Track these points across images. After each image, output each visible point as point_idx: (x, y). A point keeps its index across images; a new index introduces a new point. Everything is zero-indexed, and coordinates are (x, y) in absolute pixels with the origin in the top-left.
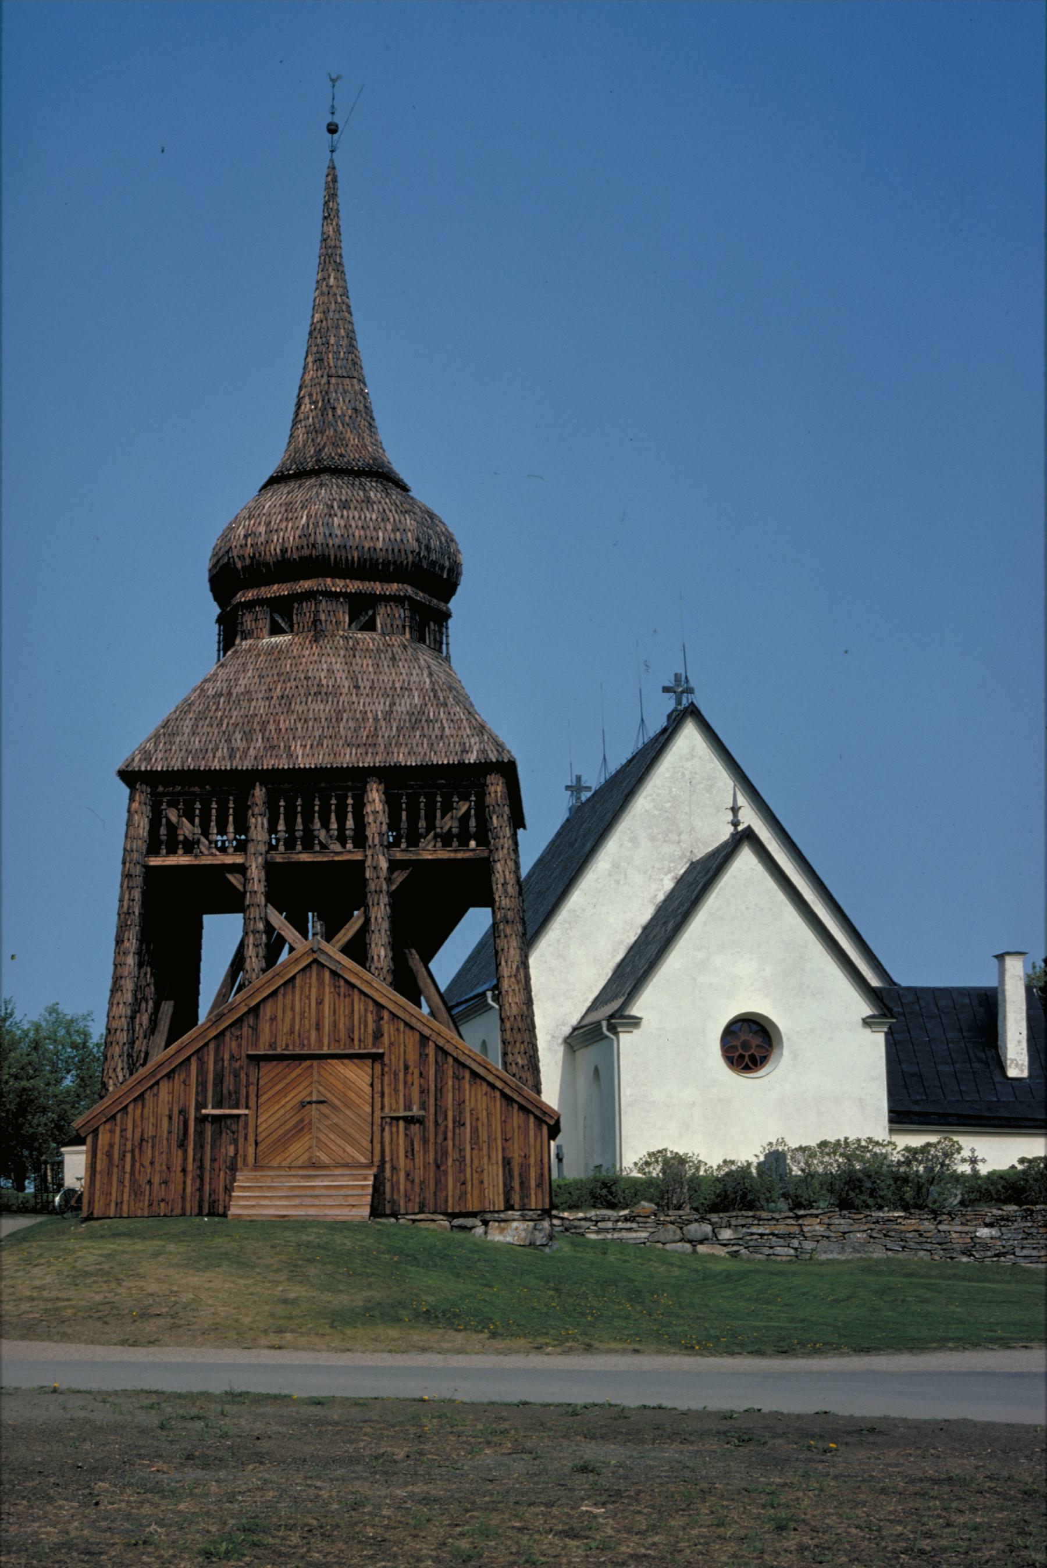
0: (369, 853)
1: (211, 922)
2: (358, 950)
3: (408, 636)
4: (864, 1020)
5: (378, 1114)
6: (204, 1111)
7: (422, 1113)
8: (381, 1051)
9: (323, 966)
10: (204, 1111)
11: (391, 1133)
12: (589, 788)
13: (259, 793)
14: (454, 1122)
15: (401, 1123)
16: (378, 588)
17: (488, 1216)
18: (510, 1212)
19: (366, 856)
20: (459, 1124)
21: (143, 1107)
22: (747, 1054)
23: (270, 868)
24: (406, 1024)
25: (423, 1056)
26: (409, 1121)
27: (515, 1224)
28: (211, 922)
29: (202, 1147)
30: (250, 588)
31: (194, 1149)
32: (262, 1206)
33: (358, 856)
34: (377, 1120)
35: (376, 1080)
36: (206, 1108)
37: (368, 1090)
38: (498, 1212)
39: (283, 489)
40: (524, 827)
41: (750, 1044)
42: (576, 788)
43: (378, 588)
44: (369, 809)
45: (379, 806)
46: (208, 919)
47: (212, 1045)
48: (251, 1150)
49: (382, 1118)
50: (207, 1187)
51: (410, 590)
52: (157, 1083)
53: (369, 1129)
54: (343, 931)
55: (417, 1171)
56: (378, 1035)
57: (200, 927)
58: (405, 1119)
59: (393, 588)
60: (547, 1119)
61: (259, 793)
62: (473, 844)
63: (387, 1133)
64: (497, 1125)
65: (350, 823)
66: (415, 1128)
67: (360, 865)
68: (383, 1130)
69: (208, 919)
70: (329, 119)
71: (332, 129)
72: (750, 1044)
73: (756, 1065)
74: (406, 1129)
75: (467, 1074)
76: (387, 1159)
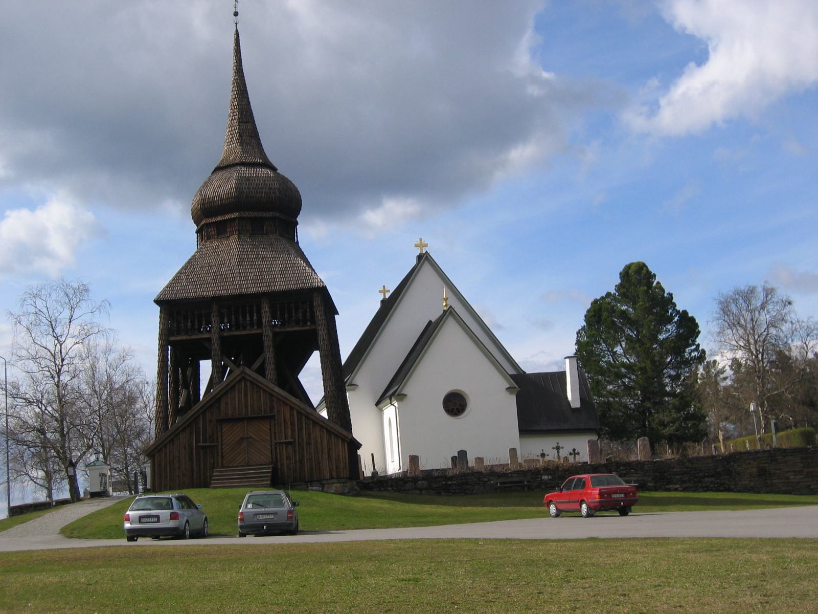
0: (264, 330)
1: (202, 363)
2: (261, 371)
3: (278, 234)
4: (506, 389)
5: (274, 442)
6: (199, 444)
7: (292, 440)
8: (274, 414)
9: (247, 380)
10: (199, 444)
11: (280, 449)
12: (389, 291)
13: (215, 308)
14: (307, 443)
15: (284, 445)
16: (265, 214)
17: (324, 482)
18: (332, 480)
19: (263, 331)
20: (309, 444)
21: (173, 444)
22: (455, 408)
23: (222, 339)
24: (284, 402)
25: (292, 415)
26: (287, 444)
27: (335, 485)
28: (202, 363)
29: (424, 516)
30: (211, 218)
31: (196, 461)
32: (224, 483)
33: (259, 331)
34: (273, 443)
35: (272, 427)
36: (200, 443)
37: (269, 431)
38: (327, 480)
39: (220, 173)
40: (338, 314)
41: (455, 404)
42: (384, 291)
43: (265, 214)
44: (263, 311)
45: (267, 309)
46: (211, 360)
47: (201, 416)
48: (220, 460)
49: (275, 443)
50: (202, 477)
51: (278, 214)
52: (179, 434)
53: (270, 448)
54: (255, 364)
55: (292, 465)
56: (272, 408)
57: (199, 366)
58: (286, 443)
59: (270, 214)
60: (347, 439)
61: (215, 308)
62: (309, 323)
63: (278, 450)
64: (325, 442)
65: (255, 318)
66: (290, 447)
67: (261, 334)
68: (276, 448)
69: (211, 360)
70: (234, 10)
71: (236, 14)
72: (455, 404)
73: (459, 412)
74: (286, 447)
75: (311, 422)
76: (279, 460)
